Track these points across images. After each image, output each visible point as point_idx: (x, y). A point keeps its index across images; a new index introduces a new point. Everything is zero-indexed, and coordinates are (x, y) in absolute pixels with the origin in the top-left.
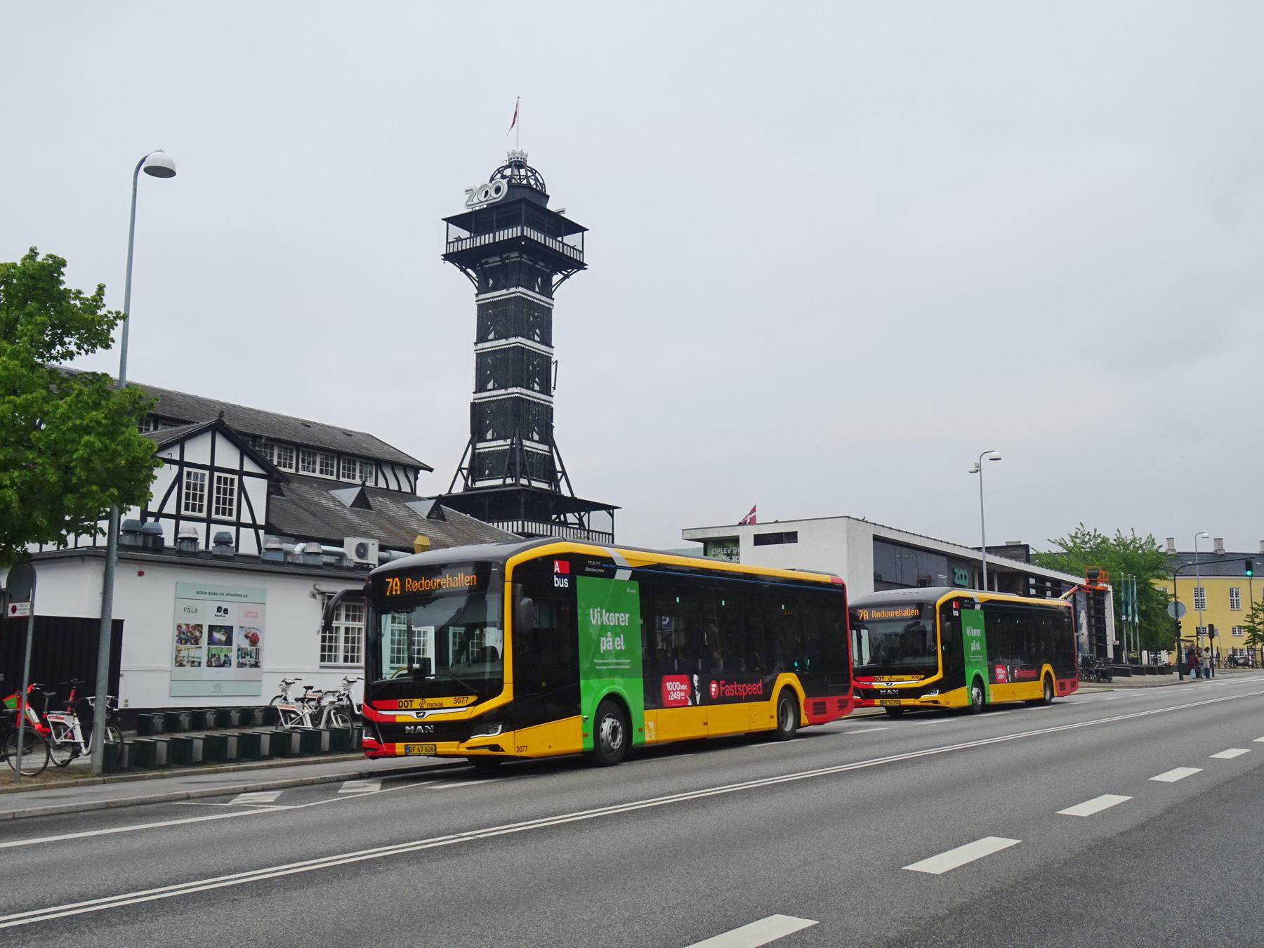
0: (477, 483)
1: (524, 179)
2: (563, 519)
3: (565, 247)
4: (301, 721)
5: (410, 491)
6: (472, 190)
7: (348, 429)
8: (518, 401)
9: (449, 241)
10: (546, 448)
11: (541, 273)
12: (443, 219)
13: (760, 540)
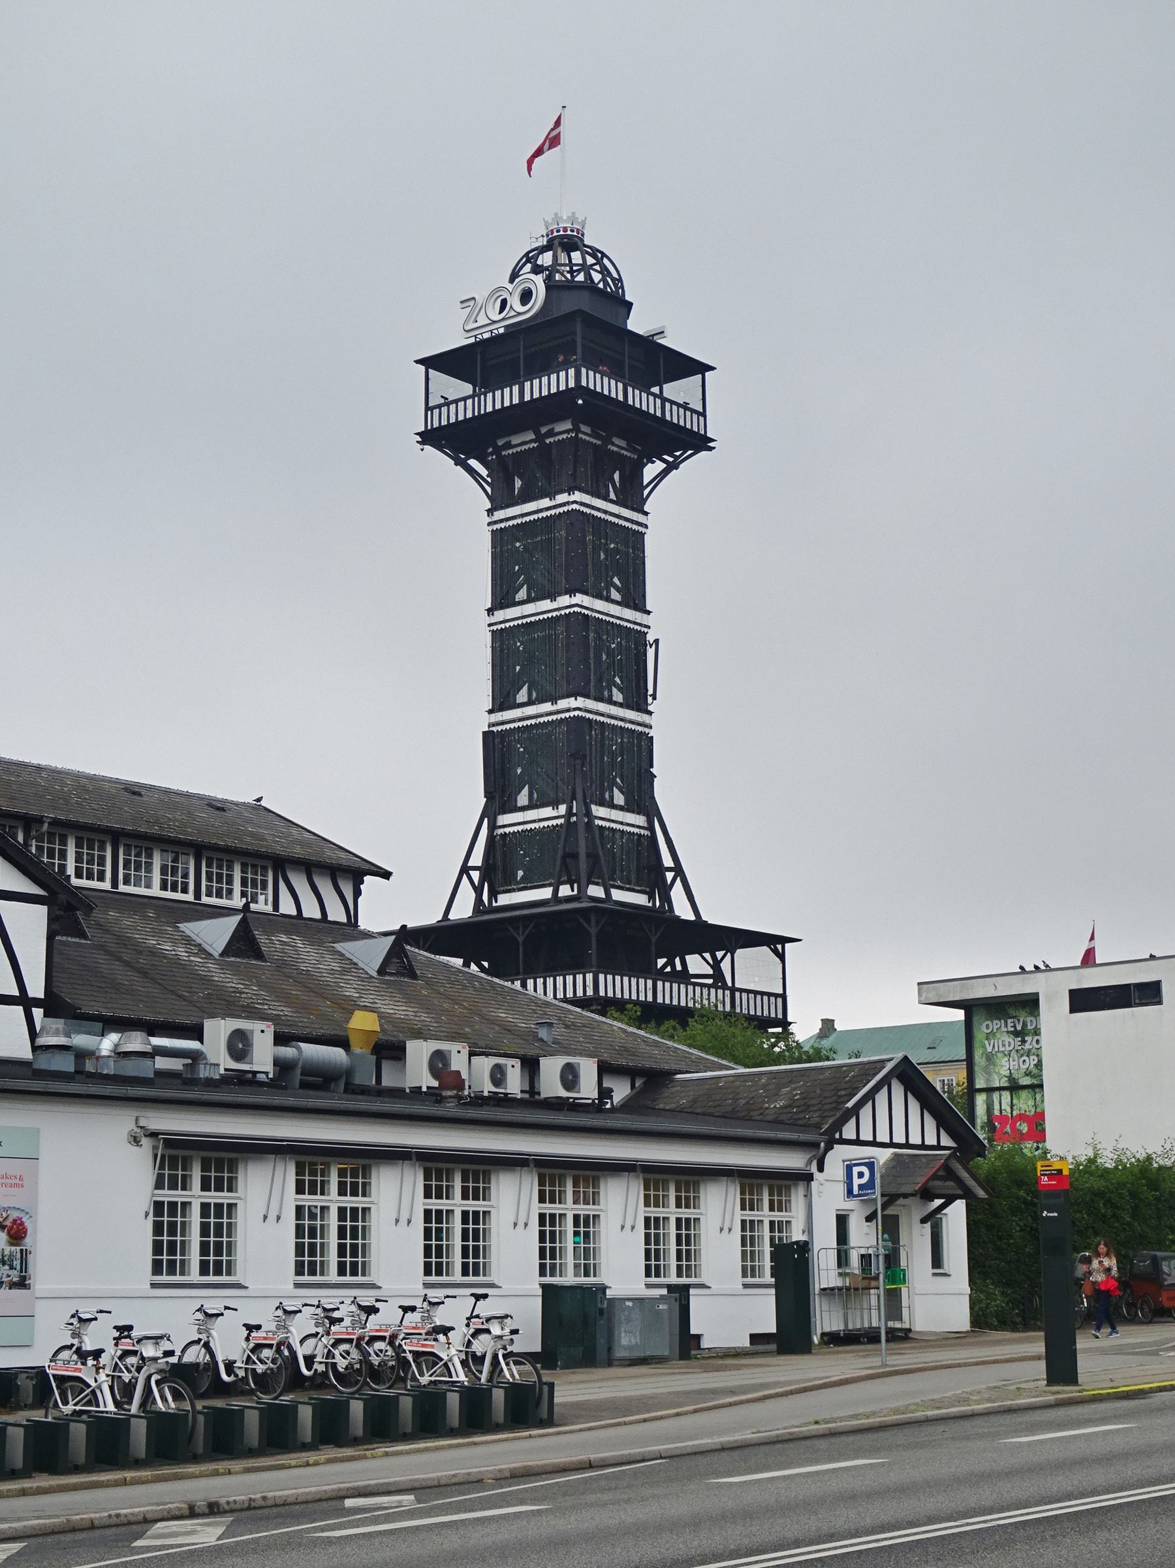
0: (500, 897)
1: (579, 271)
2: (679, 967)
3: (668, 405)
4: (94, 1399)
5: (344, 919)
6: (474, 298)
7: (219, 796)
8: (579, 725)
9: (430, 405)
10: (640, 820)
11: (618, 461)
12: (417, 362)
13: (1083, 1000)
